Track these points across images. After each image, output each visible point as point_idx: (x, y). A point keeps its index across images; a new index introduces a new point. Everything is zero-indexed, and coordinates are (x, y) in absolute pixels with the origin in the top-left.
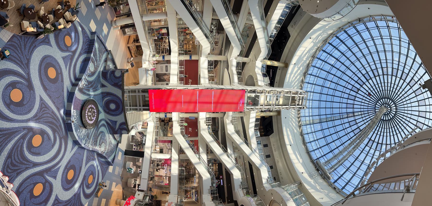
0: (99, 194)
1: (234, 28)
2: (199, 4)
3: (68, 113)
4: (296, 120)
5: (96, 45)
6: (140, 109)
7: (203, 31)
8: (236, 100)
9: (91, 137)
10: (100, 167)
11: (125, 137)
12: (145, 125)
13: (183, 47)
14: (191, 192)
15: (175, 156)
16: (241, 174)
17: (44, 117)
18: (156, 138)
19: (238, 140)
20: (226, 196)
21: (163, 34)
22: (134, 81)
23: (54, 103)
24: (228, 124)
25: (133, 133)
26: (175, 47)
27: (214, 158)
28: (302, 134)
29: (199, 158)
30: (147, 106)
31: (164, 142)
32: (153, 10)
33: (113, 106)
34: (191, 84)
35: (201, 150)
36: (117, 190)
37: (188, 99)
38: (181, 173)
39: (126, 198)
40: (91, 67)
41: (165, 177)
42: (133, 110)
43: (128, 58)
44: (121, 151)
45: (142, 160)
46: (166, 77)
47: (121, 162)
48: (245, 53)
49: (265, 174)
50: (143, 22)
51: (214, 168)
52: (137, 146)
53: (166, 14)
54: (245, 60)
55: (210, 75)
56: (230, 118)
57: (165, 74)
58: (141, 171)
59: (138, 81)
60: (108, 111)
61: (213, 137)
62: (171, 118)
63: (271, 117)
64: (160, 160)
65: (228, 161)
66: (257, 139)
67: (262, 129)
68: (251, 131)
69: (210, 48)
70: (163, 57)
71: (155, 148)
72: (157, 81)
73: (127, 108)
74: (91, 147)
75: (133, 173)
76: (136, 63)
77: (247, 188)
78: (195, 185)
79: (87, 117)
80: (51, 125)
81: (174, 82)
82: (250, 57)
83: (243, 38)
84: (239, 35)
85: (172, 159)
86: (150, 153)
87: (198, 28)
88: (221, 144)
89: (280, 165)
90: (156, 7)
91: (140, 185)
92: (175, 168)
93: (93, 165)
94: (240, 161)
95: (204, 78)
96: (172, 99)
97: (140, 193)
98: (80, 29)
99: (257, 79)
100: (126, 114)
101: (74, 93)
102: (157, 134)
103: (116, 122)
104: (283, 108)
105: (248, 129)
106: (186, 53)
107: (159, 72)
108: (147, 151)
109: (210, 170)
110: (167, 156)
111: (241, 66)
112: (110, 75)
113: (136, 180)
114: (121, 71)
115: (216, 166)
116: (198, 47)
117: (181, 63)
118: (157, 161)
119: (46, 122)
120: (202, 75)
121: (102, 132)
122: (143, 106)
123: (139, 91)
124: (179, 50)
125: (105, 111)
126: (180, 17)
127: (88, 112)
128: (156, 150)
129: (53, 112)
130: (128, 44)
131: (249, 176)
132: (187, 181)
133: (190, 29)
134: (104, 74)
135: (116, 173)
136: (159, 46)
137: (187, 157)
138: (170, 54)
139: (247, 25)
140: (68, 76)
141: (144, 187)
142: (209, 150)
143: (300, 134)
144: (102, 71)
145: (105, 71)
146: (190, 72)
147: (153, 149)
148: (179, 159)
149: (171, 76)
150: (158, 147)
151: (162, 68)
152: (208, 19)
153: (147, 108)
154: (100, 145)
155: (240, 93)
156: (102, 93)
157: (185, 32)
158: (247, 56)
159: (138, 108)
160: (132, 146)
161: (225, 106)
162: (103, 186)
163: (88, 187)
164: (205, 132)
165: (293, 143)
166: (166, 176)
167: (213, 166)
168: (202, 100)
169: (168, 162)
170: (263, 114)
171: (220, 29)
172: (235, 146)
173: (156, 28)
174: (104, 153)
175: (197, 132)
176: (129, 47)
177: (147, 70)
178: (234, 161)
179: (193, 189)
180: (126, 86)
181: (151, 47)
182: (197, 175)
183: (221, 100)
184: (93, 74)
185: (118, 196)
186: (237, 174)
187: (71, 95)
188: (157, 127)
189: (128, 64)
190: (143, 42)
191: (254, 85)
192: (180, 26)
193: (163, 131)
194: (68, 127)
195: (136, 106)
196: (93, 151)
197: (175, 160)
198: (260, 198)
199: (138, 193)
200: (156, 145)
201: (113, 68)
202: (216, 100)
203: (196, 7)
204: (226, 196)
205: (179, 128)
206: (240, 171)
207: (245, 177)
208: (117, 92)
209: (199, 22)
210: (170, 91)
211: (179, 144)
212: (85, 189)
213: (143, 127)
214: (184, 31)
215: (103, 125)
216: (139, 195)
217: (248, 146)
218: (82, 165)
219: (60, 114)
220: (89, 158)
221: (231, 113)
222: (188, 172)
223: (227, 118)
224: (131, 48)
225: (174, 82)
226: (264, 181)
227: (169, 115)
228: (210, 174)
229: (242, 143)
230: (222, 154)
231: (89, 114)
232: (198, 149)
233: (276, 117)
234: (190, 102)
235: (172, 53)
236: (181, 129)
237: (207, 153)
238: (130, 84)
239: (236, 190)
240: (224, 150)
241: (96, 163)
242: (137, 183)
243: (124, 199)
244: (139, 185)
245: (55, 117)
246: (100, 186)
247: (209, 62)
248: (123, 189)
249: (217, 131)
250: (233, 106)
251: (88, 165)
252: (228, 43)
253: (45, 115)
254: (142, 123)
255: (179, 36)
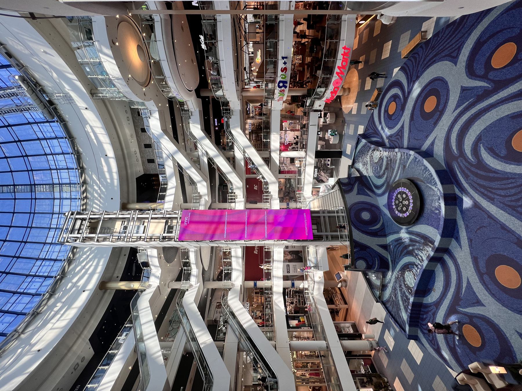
0: (376, 93)
1: (191, 332)
2: (243, 362)
3: (452, 200)
4: (92, 195)
5: (405, 316)
6: (324, 213)
7: (239, 323)
8: (193, 227)
9: (399, 168)
10: (377, 129)
11: (343, 173)
12: (316, 191)
13: (266, 299)
14: (254, 114)
15: (275, 156)
16: (190, 129)
17: (515, 187)
18: (300, 174)
19: (193, 173)
20: (211, 106)
21: (294, 318)
22: (334, 252)
23: (490, 216)
24: (205, 195)
25: (332, 181)
26: (278, 301)
27: (225, 152)
28: (82, 170)
29: (244, 152)
30: (315, 218)
31: (289, 172)
32: (311, 356)
33: (366, 216)
34: (254, 247)
35: (243, 163)
36: (349, 106)
37: (258, 228)
38: (267, 135)
39: (336, 99)
40: (412, 279)
41: (288, 129)
42: (333, 212)
43: (346, 287)
44: (347, 156)
45: (317, 147)
46: (289, 257)
47: (346, 142)
48: (178, 295)
49: (154, 124)
50: (325, 339)
51: (225, 140)
52: (325, 164)
53: (292, 348)
54: (177, 285)
55: (229, 260)
56: (203, 201)
57: (290, 261)
58: (318, 134)
59: (328, 253)
60: (373, 209)
61: (226, 178)
62: (280, 202)
63: (140, 200)
64: (294, 149)
65: (207, 147)
66: (165, 171)
67: (155, 185)
68: (172, 185)
69: (229, 298)
70: (293, 285)
71: (300, 164)
72: (301, 251)
73: (344, 214)
74: (398, 154)
75: (329, 131)
76: (333, 279)
77: (183, 110)
78: (249, 121)
79: (411, 197)
80: (491, 175)
81: (278, 250)
82: (169, 290)
83: (179, 318)
84: (184, 321)
85: (278, 152)
86: (308, 159)
87: (245, 326)
88: (216, 168)
89: (128, 131)
90: (306, 360)
91: (319, 117)
92: (275, 141)
93: (390, 128)
94: (190, 145)
95: (237, 257)
96: (279, 228)
97: (319, 108)
98: (446, 354)
99: (159, 258)
100: (343, 205)
101: (443, 236)
102: (299, 181)
103: (358, 193)
104: (115, 214)
105: (176, 187)
106: (262, 291)
107: (298, 264)
108: (311, 160)
109: (230, 138)
110: (285, 154)
111: (183, 275)
112: (374, 264)
113: (324, 123)
114: (355, 268)
115: (223, 142)
116: (246, 299)
117: (268, 276)
118: (298, 148)
119: (508, 179)
120: (240, 260)
121: (380, 177)
122: (319, 217)
123: (327, 237)
124: (271, 294)
125: (378, 208)
126: (271, 342)
127: (408, 205)
128: (300, 161)
129: (491, 200)
130: (347, 309)
131: (179, 125)
132: (259, 125)
133: (256, 325)
134: (384, 267)
135: (352, 127)
136: (299, 301)
137: (260, 155)
138: (284, 289)
139: (170, 339)
140: (462, 267)
141: (314, 117)
142: (231, 162)
143: (86, 171)
144: (388, 270)
145: (384, 270)
146: (256, 262)
147: (304, 162)
148: (270, 152)
149: (282, 258)
150: (296, 165)
151: (295, 269)
152: (231, 340)
153: (314, 215)
154: (381, 159)
155: (186, 236)
156: (385, 236)
157: (263, 320)
158: (174, 292)
159: (326, 215)
160: (332, 164)
161: (207, 219)
162: (370, 106)
163: (395, 97)
164: (237, 183)
165: (102, 160)
166: (286, 131)
167: (228, 143)
168: (240, 227)
169: (285, 147)
170: (153, 205)
171: (213, 328)
172: (197, 165)
173: (306, 329)
174: (374, 150)
175: (247, 184)
176: (346, 303)
177: (317, 267)
178: (199, 146)
179: (253, 117)
180: (346, 246)
181: (312, 301)
182: (247, 132)
183: (213, 226)
184: (408, 267)
185: (347, 98)
186: (196, 129)
187: (450, 230)
188: (300, 189)
189: (346, 279)
190: (324, 310)
191: (164, 248)
192: (270, 329)
193: (291, 185)
194: (446, 176)
195: (329, 217)
196: (392, 148)
197: (274, 151)
198: (165, 94)
199: (322, 108)
200: (300, 167)
201: (370, 274)
202: (221, 226)
203: (247, 358)
204: (211, 106)
205: (270, 190)
206: (191, 134)
207: (184, 124)
208: (358, 236)
209: (244, 336)
210: (283, 237)
211: (270, 169)
212: (400, 93)
213: (318, 190)
214: (265, 320)
215: (378, 187)
216: (320, 106)
217: (178, 163)
218: (410, 125)
219: (472, 198)
220: (398, 137)
221: (202, 208)
222: (259, 136)
223: (206, 202)
224: (342, 302)
225: (278, 250)
226: (156, 115)
227: (284, 205)
228: (231, 133)
229: (188, 168)
230: (216, 156)
231: (406, 203)
232: (246, 164)
233: (130, 201)
234: (256, 223)
235: (281, 291)
236: (268, 188)
237: (234, 158)
238: (341, 248)
239: (197, 110)
240: (211, 161)
241: (386, 132)
242: (322, 120)
243: (339, 97)
244: (321, 117)
245: (482, 190)
246: (377, 104)
247: (230, 279)
248: (341, 109)
249: (220, 185)
250: (196, 218)
251: (398, 126)
252: (202, 308)
253: (513, 191)
254: (320, 194)
255: (272, 315)
